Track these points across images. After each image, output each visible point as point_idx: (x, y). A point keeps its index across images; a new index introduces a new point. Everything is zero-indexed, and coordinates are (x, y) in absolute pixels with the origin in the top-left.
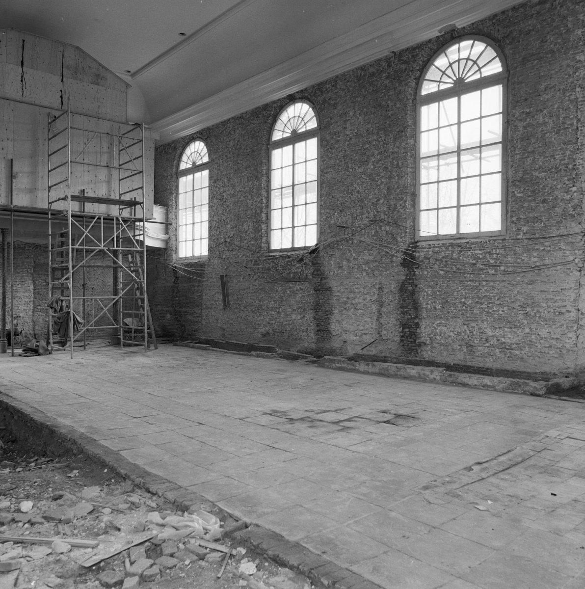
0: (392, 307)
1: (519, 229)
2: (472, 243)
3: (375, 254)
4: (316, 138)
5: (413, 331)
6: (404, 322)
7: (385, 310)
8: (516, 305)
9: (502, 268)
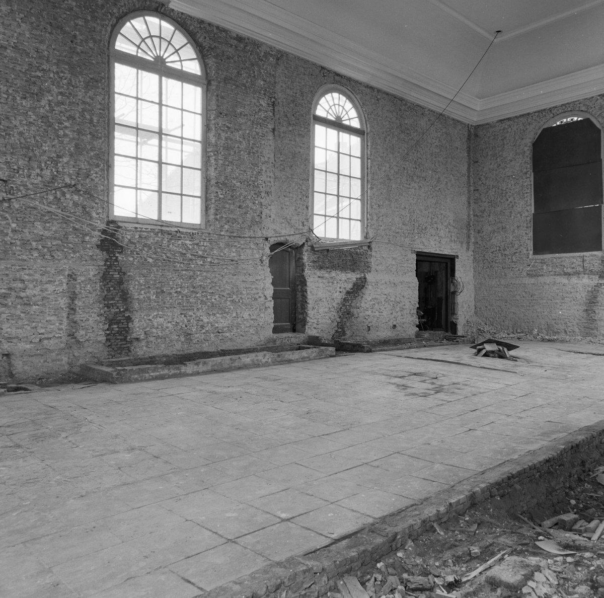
0: (92, 299)
1: (222, 227)
2: (182, 233)
3: (54, 229)
4: (117, 65)
5: (123, 326)
6: (111, 317)
7: (80, 304)
8: (225, 294)
9: (209, 260)
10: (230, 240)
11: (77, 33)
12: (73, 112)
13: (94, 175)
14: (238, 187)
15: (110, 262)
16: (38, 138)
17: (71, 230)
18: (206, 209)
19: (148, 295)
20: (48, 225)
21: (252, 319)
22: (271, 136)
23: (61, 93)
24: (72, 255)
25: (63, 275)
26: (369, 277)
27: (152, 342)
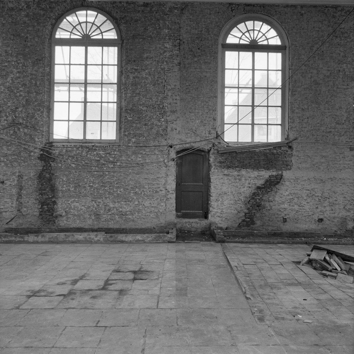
2: (97, 147)
3: (13, 149)
5: (51, 207)
6: (43, 201)
7: (25, 192)
8: (129, 188)
9: (118, 164)
10: (137, 149)
11: (28, 35)
12: (25, 81)
13: (37, 116)
14: (144, 111)
15: (46, 167)
16: (5, 100)
17: (22, 149)
18: (119, 129)
19: (68, 188)
20: (10, 147)
21: (153, 207)
22: (176, 69)
23: (19, 72)
24: (23, 164)
25: (15, 176)
26: (286, 174)
27: (70, 218)
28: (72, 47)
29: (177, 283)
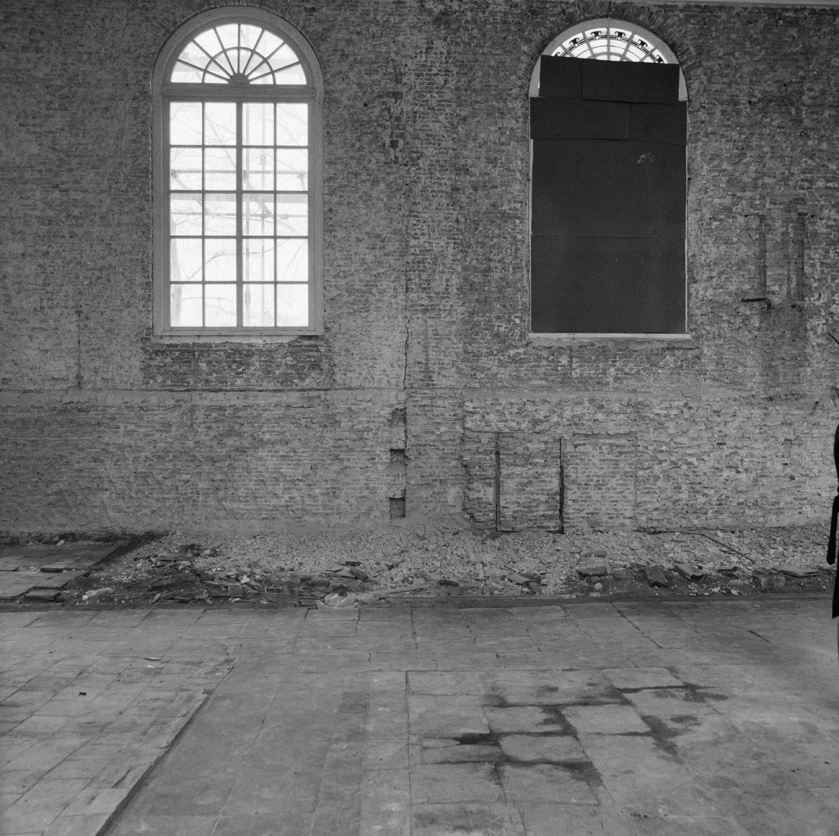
28: (208, 105)
29: (362, 726)
